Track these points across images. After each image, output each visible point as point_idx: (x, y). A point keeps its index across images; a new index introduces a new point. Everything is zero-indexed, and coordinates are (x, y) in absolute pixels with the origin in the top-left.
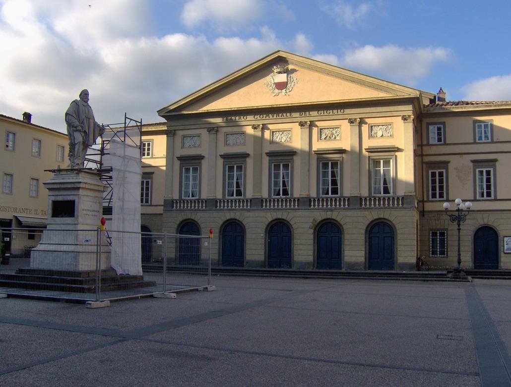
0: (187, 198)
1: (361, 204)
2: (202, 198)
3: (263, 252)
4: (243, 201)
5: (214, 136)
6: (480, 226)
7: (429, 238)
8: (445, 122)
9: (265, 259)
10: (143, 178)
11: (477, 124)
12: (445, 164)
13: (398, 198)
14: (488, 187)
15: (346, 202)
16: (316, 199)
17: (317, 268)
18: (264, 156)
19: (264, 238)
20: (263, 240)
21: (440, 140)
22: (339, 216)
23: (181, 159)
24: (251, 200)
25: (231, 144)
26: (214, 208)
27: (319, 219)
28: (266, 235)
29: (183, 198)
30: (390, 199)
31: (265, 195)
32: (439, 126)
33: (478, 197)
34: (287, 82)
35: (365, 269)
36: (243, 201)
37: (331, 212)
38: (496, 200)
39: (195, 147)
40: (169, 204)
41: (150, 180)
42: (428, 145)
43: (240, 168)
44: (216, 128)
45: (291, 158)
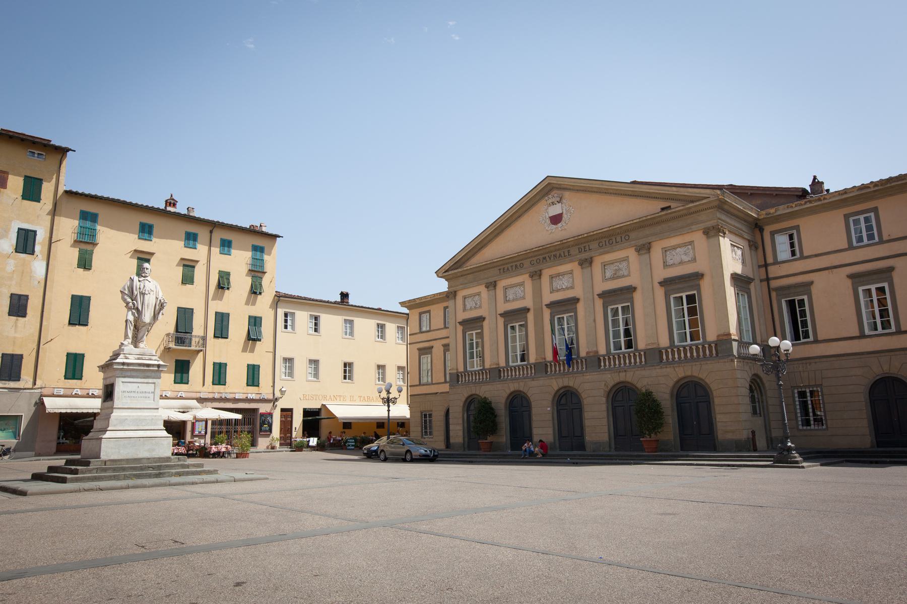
2: (486, 368)
5: (492, 292)
6: (878, 378)
7: (794, 401)
8: (798, 226)
11: (851, 219)
12: (806, 287)
14: (884, 313)
18: (544, 307)
21: (793, 253)
28: (553, 408)
29: (511, 364)
32: (790, 232)
33: (867, 332)
34: (562, 213)
37: (624, 373)
38: (816, 341)
39: (475, 308)
42: (776, 262)
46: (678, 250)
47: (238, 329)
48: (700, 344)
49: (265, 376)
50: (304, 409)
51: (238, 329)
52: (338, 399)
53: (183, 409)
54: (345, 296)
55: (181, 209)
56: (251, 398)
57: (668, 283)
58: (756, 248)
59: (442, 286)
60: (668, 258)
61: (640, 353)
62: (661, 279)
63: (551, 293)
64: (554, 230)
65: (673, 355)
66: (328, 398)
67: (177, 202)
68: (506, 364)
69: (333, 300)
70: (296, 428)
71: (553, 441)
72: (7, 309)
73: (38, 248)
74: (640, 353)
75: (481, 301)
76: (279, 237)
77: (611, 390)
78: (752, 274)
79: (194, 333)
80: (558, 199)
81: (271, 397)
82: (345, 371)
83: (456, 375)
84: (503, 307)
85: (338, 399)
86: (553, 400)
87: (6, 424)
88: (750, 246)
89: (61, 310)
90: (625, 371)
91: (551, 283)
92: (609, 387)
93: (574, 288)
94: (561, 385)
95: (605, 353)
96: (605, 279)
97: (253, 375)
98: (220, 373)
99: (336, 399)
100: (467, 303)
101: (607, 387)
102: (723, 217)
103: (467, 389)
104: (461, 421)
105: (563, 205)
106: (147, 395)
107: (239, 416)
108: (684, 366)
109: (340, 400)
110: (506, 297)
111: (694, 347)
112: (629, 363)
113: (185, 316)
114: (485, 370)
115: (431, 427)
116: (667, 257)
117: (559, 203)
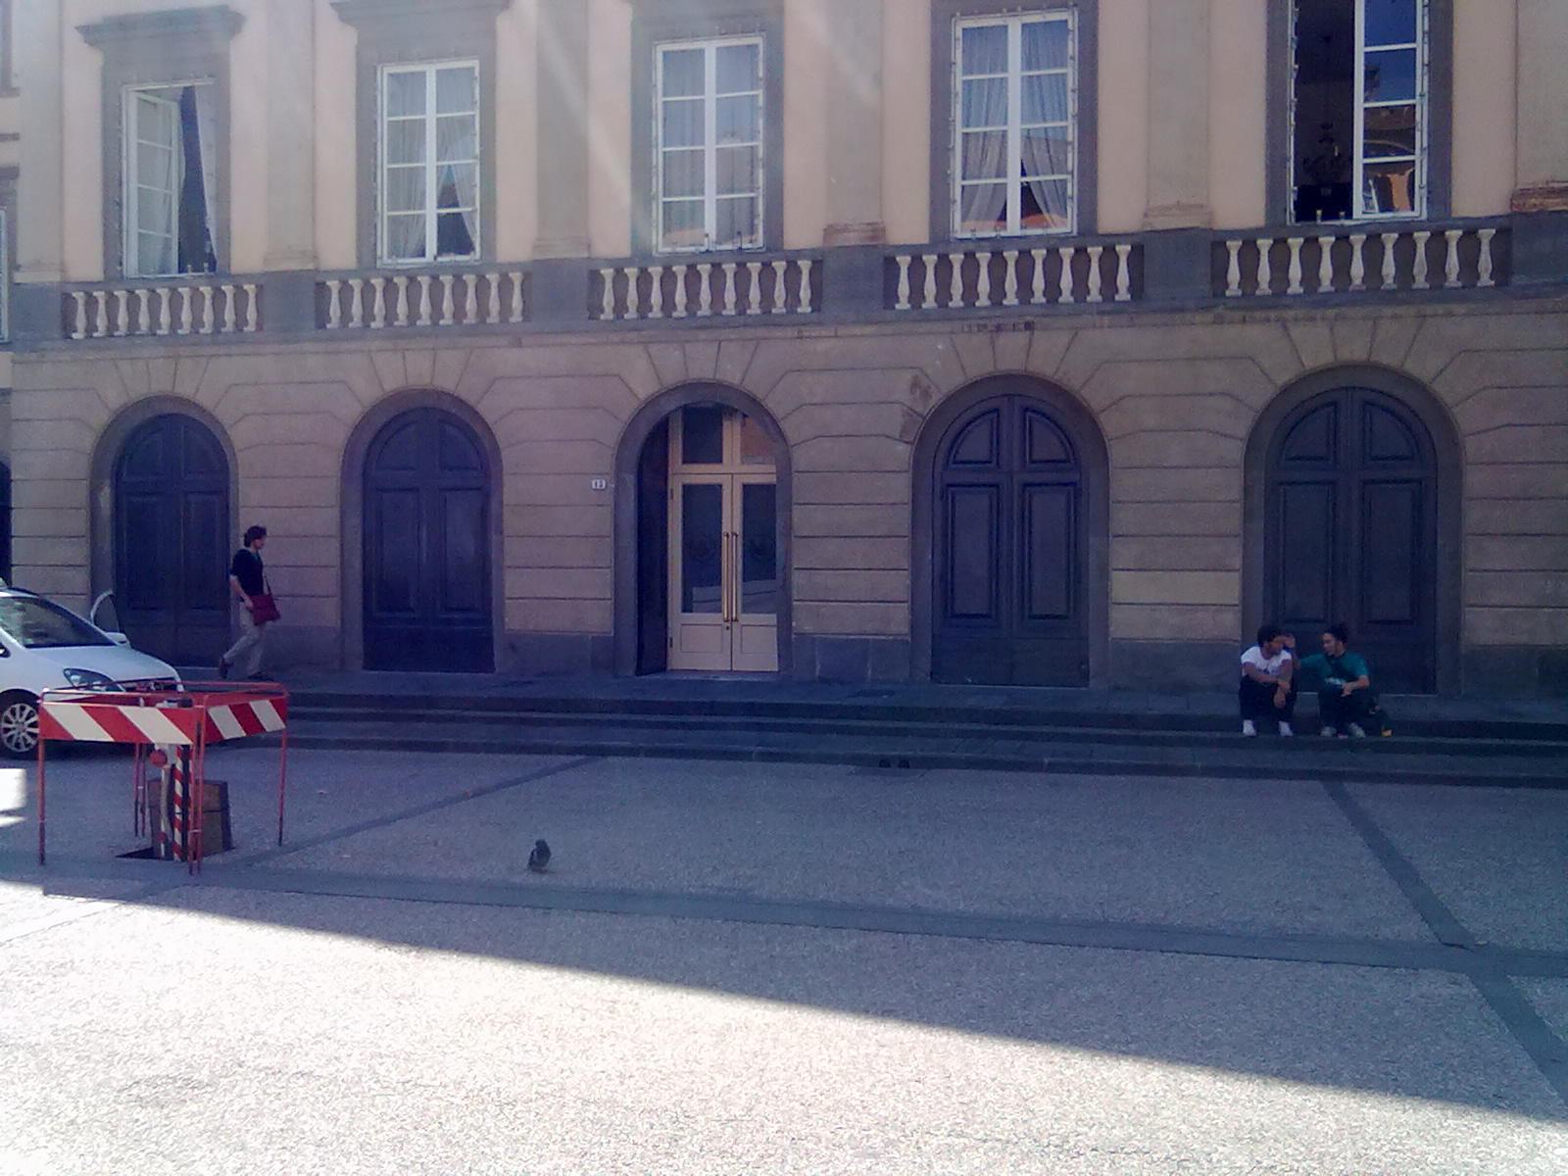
9: (914, 626)
13: (1471, 231)
16: (930, 260)
19: (609, 499)
20: (606, 514)
28: (619, 481)
37: (1022, 338)
48: (471, 269)
61: (131, 292)
65: (1280, 266)
68: (359, 259)
77: (938, 412)
90: (1029, 326)
92: (935, 399)
94: (673, 375)
95: (925, 240)
108: (1336, 318)
111: (447, 280)
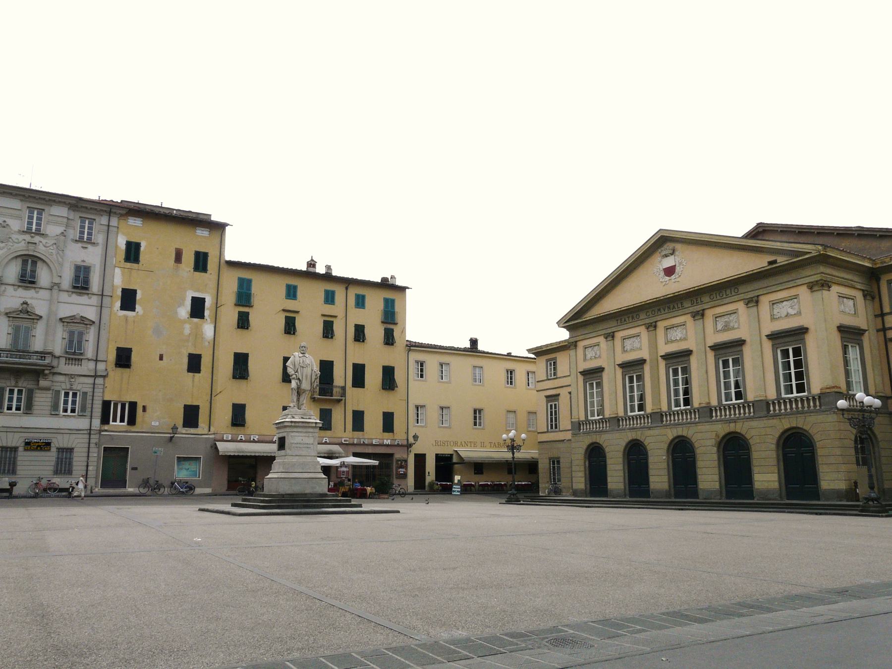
0: (593, 418)
1: (769, 410)
2: (605, 417)
3: (666, 479)
4: (808, 399)
5: (610, 343)
10: (548, 402)
15: (817, 401)
17: (727, 498)
19: (666, 461)
22: (602, 439)
23: (714, 348)
24: (819, 397)
25: (628, 350)
26: (616, 428)
27: (722, 434)
28: (668, 456)
29: (589, 418)
30: (792, 401)
31: (665, 408)
34: (675, 265)
35: (781, 499)
36: (808, 399)
39: (595, 358)
40: (577, 426)
41: (557, 403)
43: (736, 362)
44: (701, 312)
45: (688, 359)
46: (785, 303)
47: (373, 377)
49: (398, 423)
50: (436, 454)
51: (373, 377)
52: (469, 445)
53: (238, 452)
54: (474, 342)
55: (320, 269)
56: (387, 444)
57: (774, 337)
58: (873, 298)
59: (564, 335)
60: (775, 312)
62: (768, 333)
63: (666, 344)
64: (668, 282)
66: (459, 444)
67: (316, 262)
69: (462, 346)
70: (429, 473)
71: (668, 489)
72: (185, 366)
73: (207, 313)
74: (748, 405)
75: (600, 351)
76: (408, 288)
78: (866, 325)
79: (334, 384)
80: (671, 252)
81: (405, 443)
82: (475, 418)
83: (578, 425)
84: (622, 358)
85: (469, 445)
86: (668, 449)
87: (189, 465)
88: (865, 296)
89: (226, 365)
91: (666, 335)
93: (687, 340)
96: (717, 331)
97: (388, 422)
98: (358, 419)
99: (467, 446)
100: (587, 353)
101: (718, 437)
102: (829, 271)
103: (588, 437)
104: (582, 468)
105: (676, 257)
106: (308, 446)
107: (376, 463)
109: (471, 446)
110: (624, 347)
112: (796, 408)
113: (326, 367)
114: (748, 403)
115: (559, 474)
116: (774, 310)
117: (672, 255)
